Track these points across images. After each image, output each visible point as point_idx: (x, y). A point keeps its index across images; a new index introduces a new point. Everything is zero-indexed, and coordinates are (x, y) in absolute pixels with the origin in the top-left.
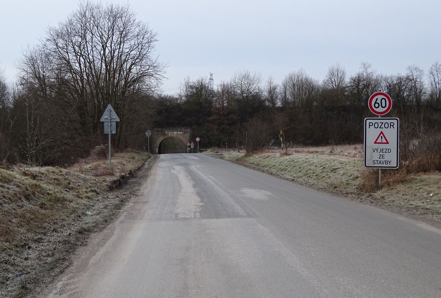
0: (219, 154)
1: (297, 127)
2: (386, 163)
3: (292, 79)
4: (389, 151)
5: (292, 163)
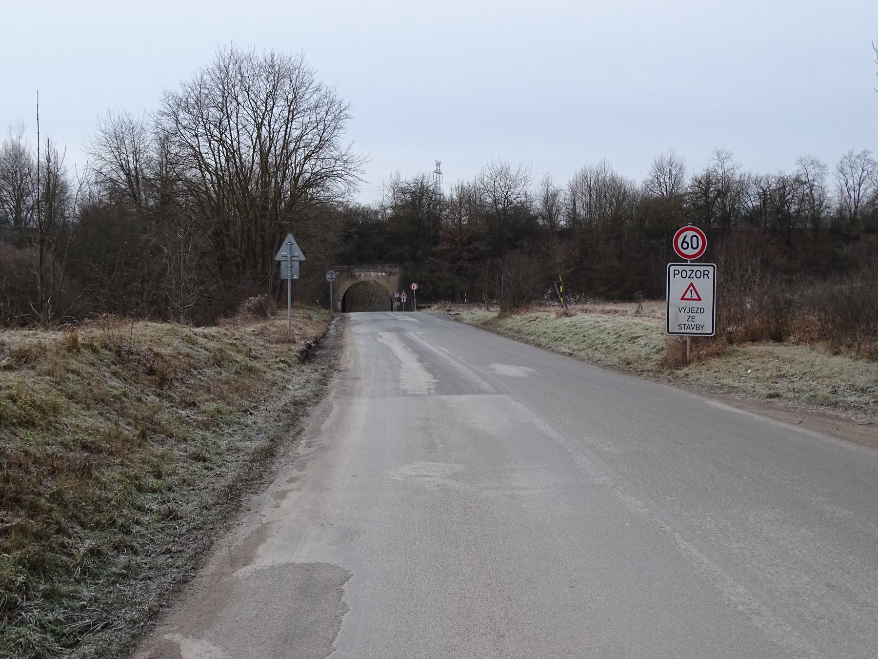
0: (452, 313)
1: (594, 267)
2: (698, 328)
3: (586, 178)
4: (702, 311)
5: (573, 329)
